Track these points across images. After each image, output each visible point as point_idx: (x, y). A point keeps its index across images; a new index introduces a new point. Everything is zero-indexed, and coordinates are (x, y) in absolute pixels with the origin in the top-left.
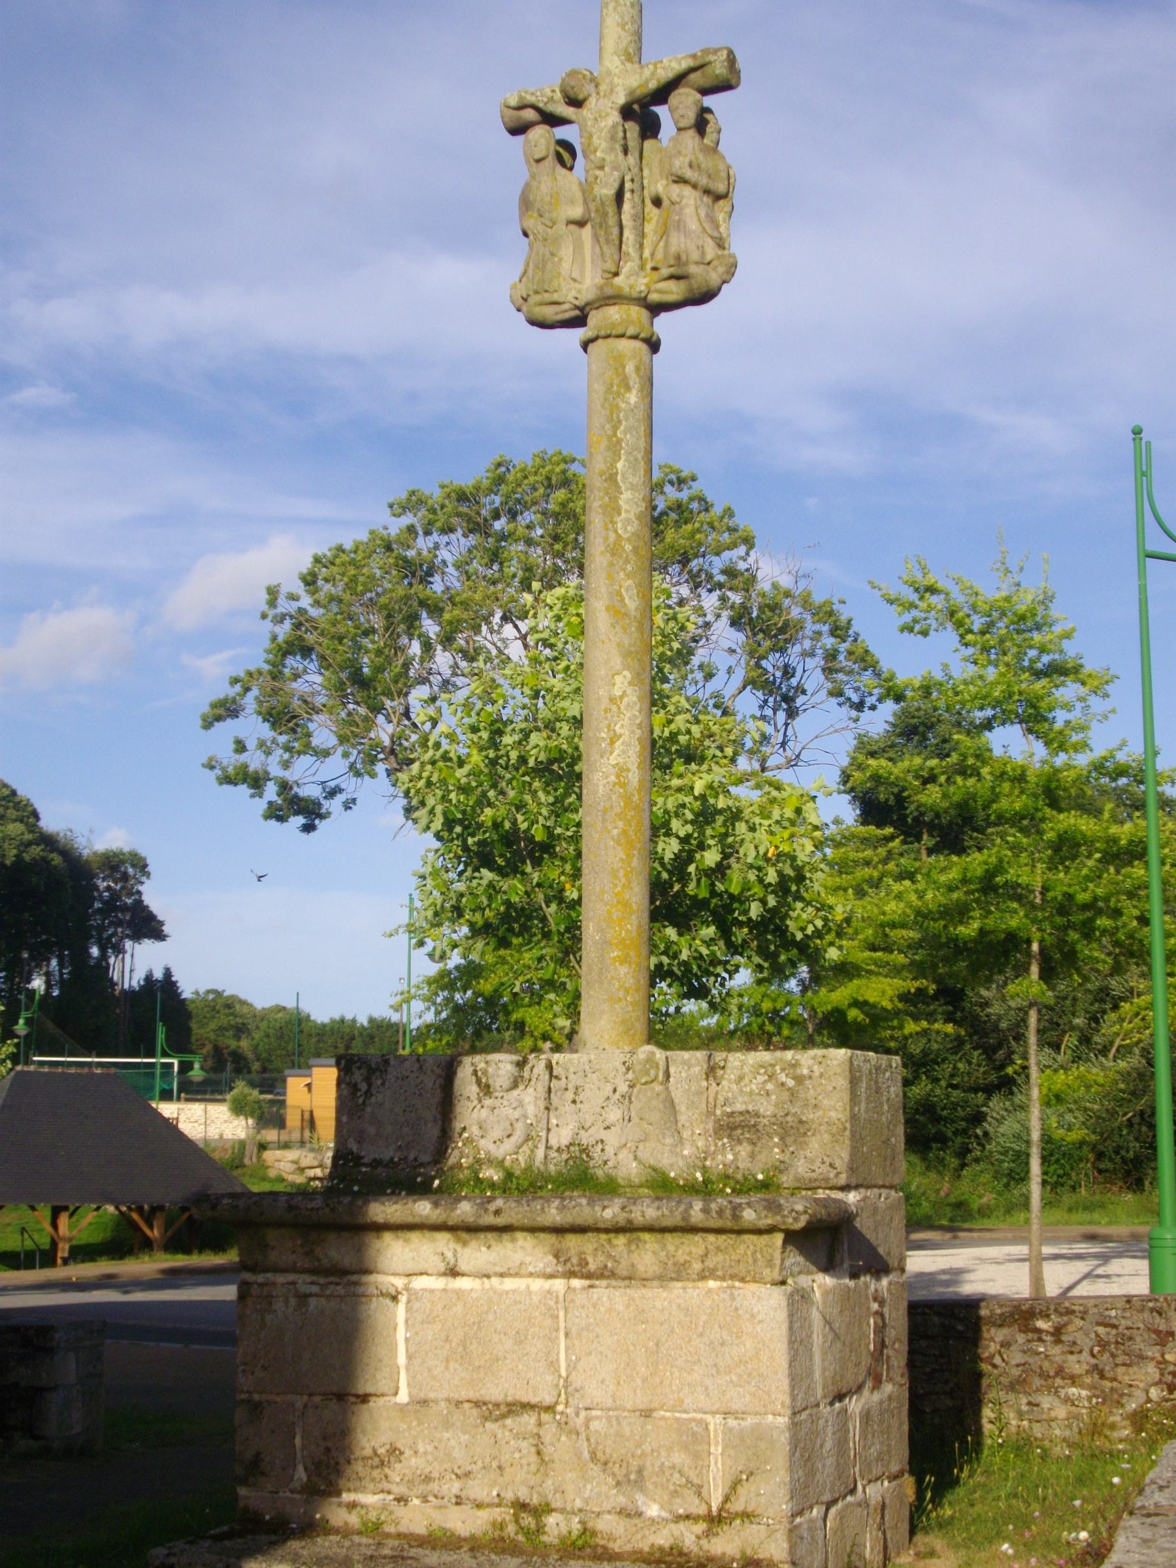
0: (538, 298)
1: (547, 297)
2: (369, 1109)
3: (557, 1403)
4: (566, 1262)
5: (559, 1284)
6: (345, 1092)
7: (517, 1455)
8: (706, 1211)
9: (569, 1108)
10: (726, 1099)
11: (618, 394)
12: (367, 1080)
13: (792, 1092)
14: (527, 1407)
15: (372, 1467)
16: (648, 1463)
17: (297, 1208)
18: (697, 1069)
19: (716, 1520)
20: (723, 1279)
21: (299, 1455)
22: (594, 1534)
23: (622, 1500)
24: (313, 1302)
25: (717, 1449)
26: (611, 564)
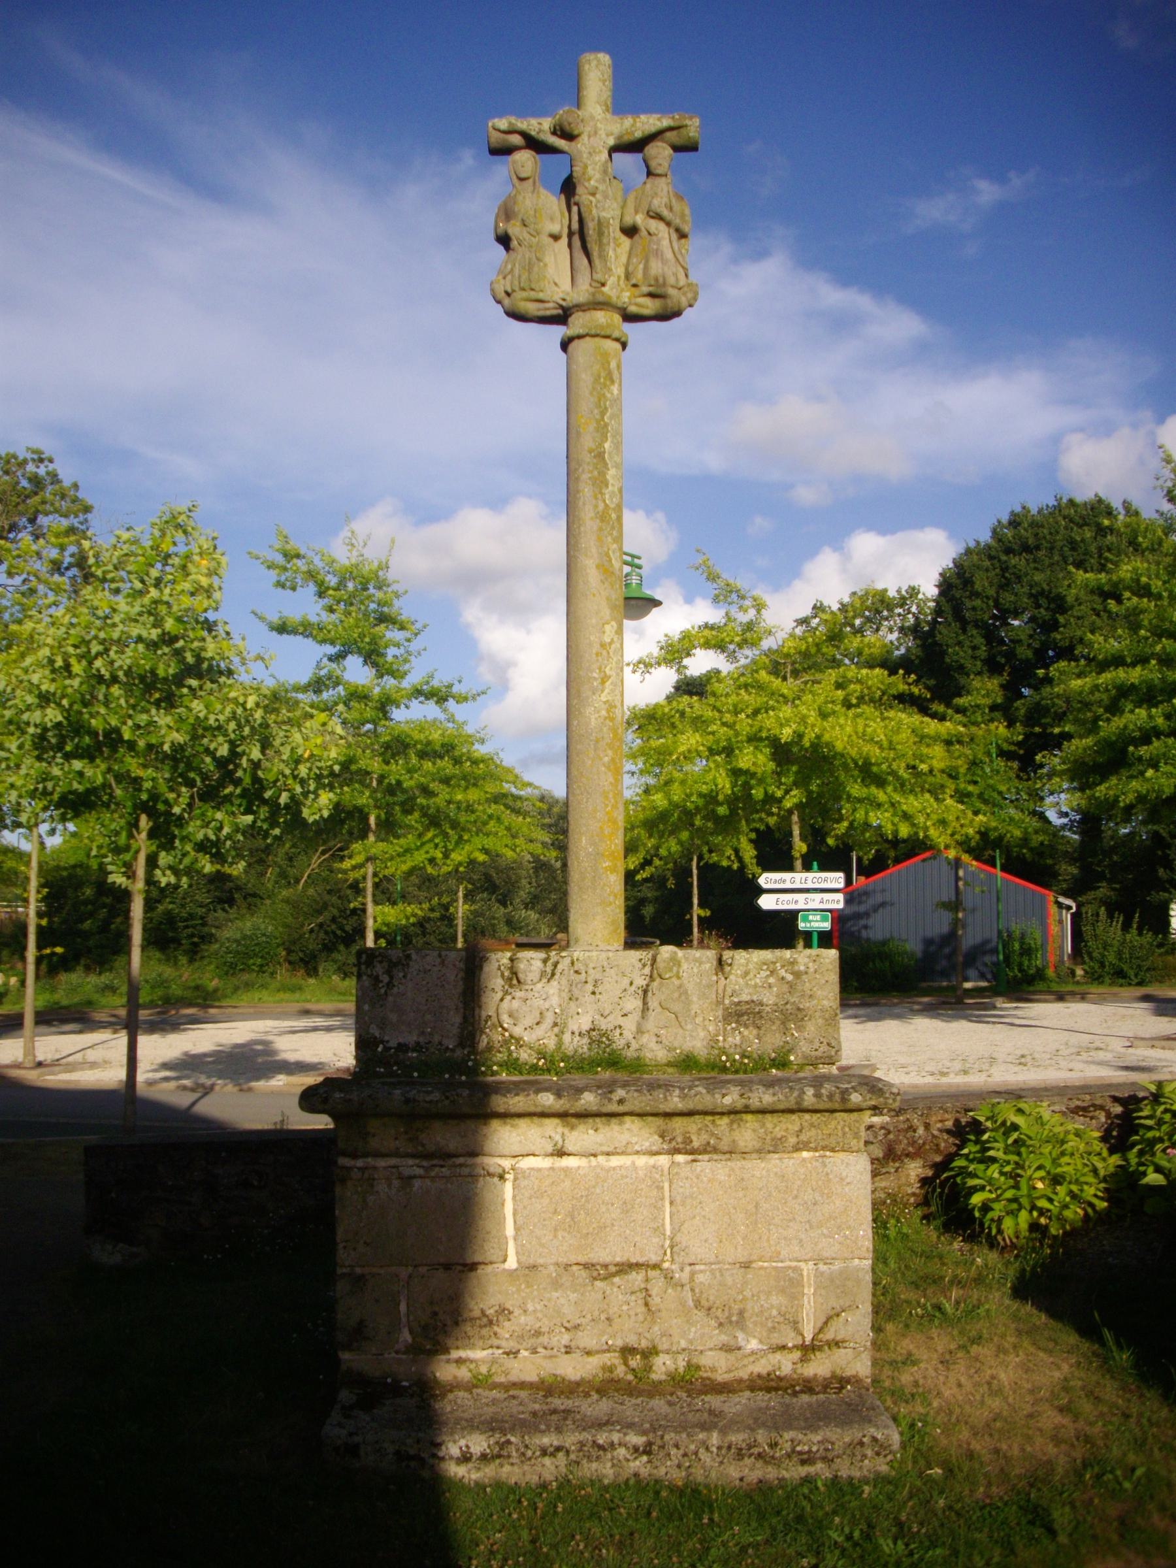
0: (524, 294)
1: (533, 295)
2: (390, 999)
3: (663, 1261)
4: (671, 1140)
5: (664, 1160)
6: (367, 984)
7: (625, 1308)
8: (818, 1095)
9: (589, 998)
10: (734, 991)
11: (605, 385)
12: (388, 972)
13: (791, 985)
14: (638, 1266)
15: (481, 1327)
16: (749, 1307)
17: (415, 1100)
18: (708, 966)
19: (808, 1350)
20: (815, 1150)
21: (404, 1320)
22: (698, 1368)
23: (724, 1338)
24: (417, 1183)
25: (809, 1291)
26: (601, 529)
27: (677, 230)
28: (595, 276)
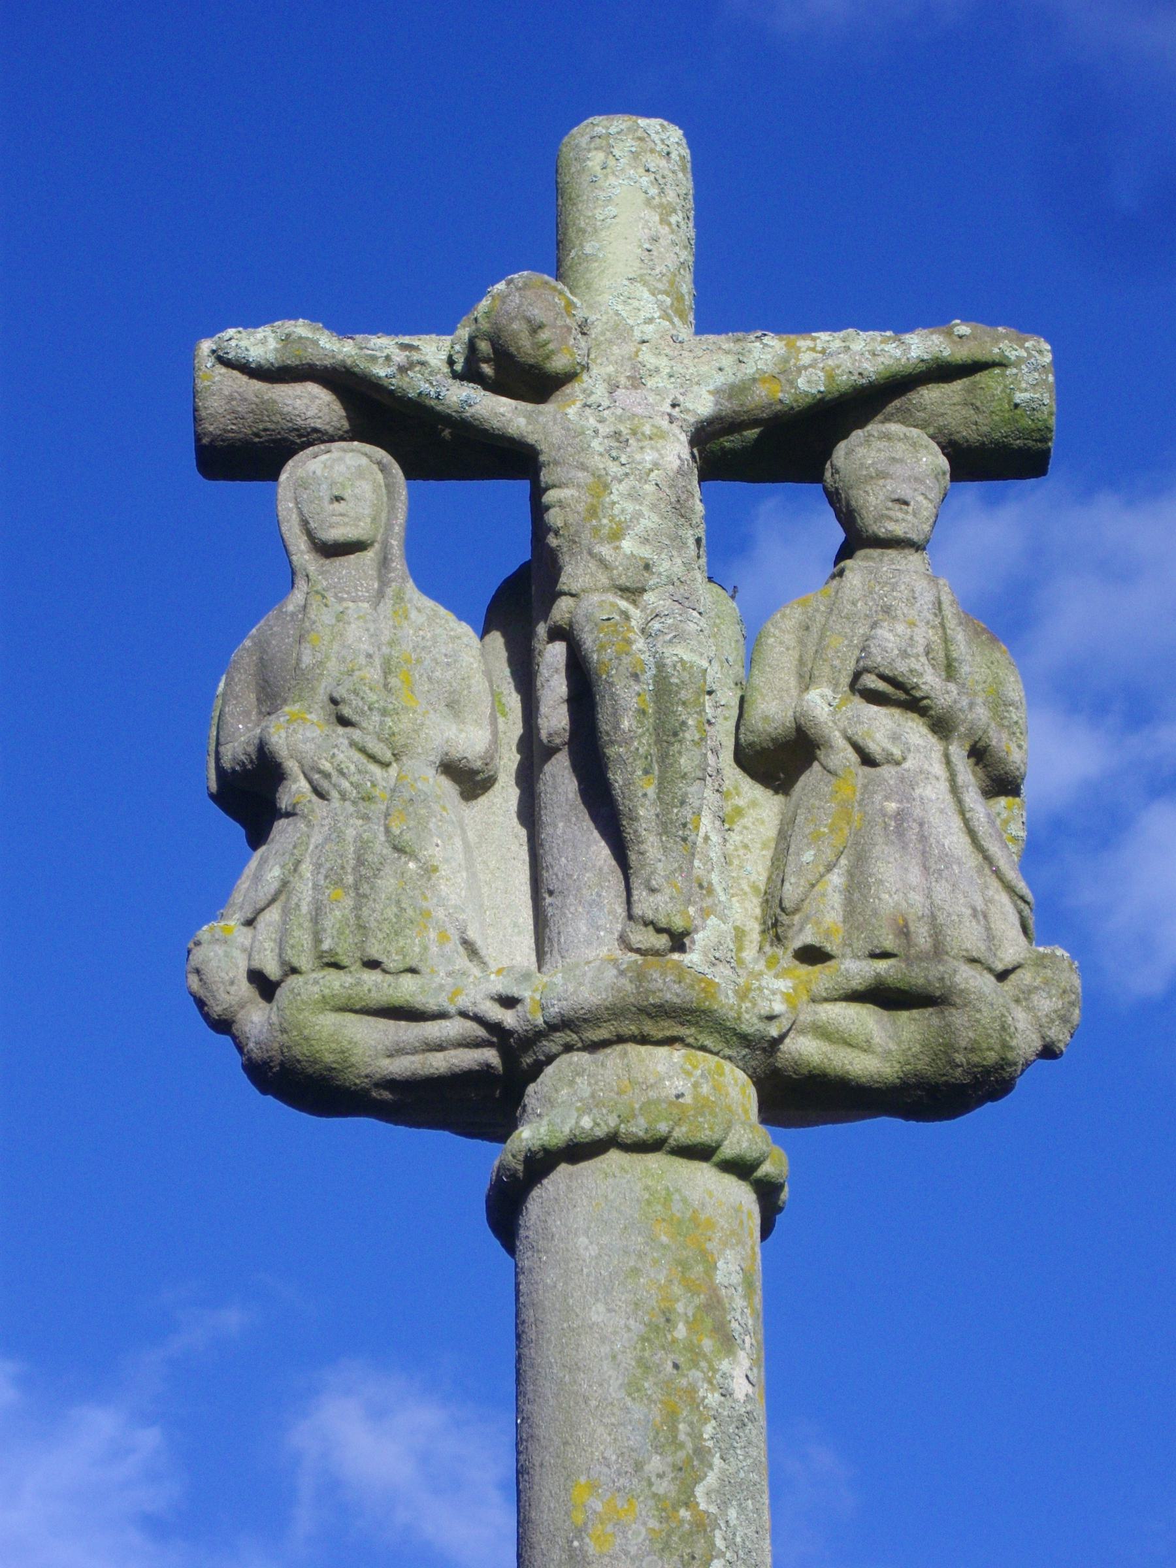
0: (335, 981)
27: (979, 753)
28: (645, 904)
